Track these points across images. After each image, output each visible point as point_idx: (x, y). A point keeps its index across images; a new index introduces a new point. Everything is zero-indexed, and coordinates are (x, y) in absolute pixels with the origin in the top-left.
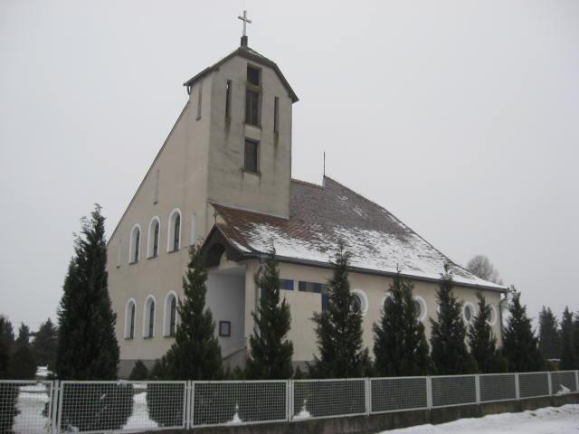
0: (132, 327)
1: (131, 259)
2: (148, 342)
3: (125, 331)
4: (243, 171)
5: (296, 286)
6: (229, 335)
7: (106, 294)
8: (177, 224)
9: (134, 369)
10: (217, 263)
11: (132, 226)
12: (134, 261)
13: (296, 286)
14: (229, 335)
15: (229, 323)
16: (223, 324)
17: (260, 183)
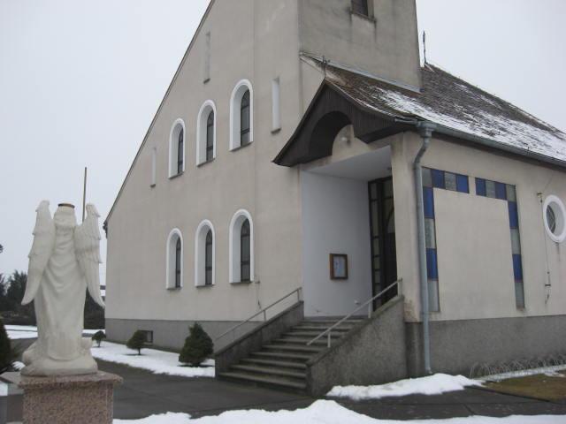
0: (178, 272)
1: (172, 170)
2: (205, 293)
3: (167, 283)
4: (350, 13)
5: (472, 186)
6: (345, 278)
7: (222, 412)
8: (209, 243)
9: (188, 339)
10: (327, 152)
11: (174, 120)
12: (176, 173)
13: (472, 186)
14: (345, 278)
15: (345, 256)
16: (336, 260)
17: (375, 33)
